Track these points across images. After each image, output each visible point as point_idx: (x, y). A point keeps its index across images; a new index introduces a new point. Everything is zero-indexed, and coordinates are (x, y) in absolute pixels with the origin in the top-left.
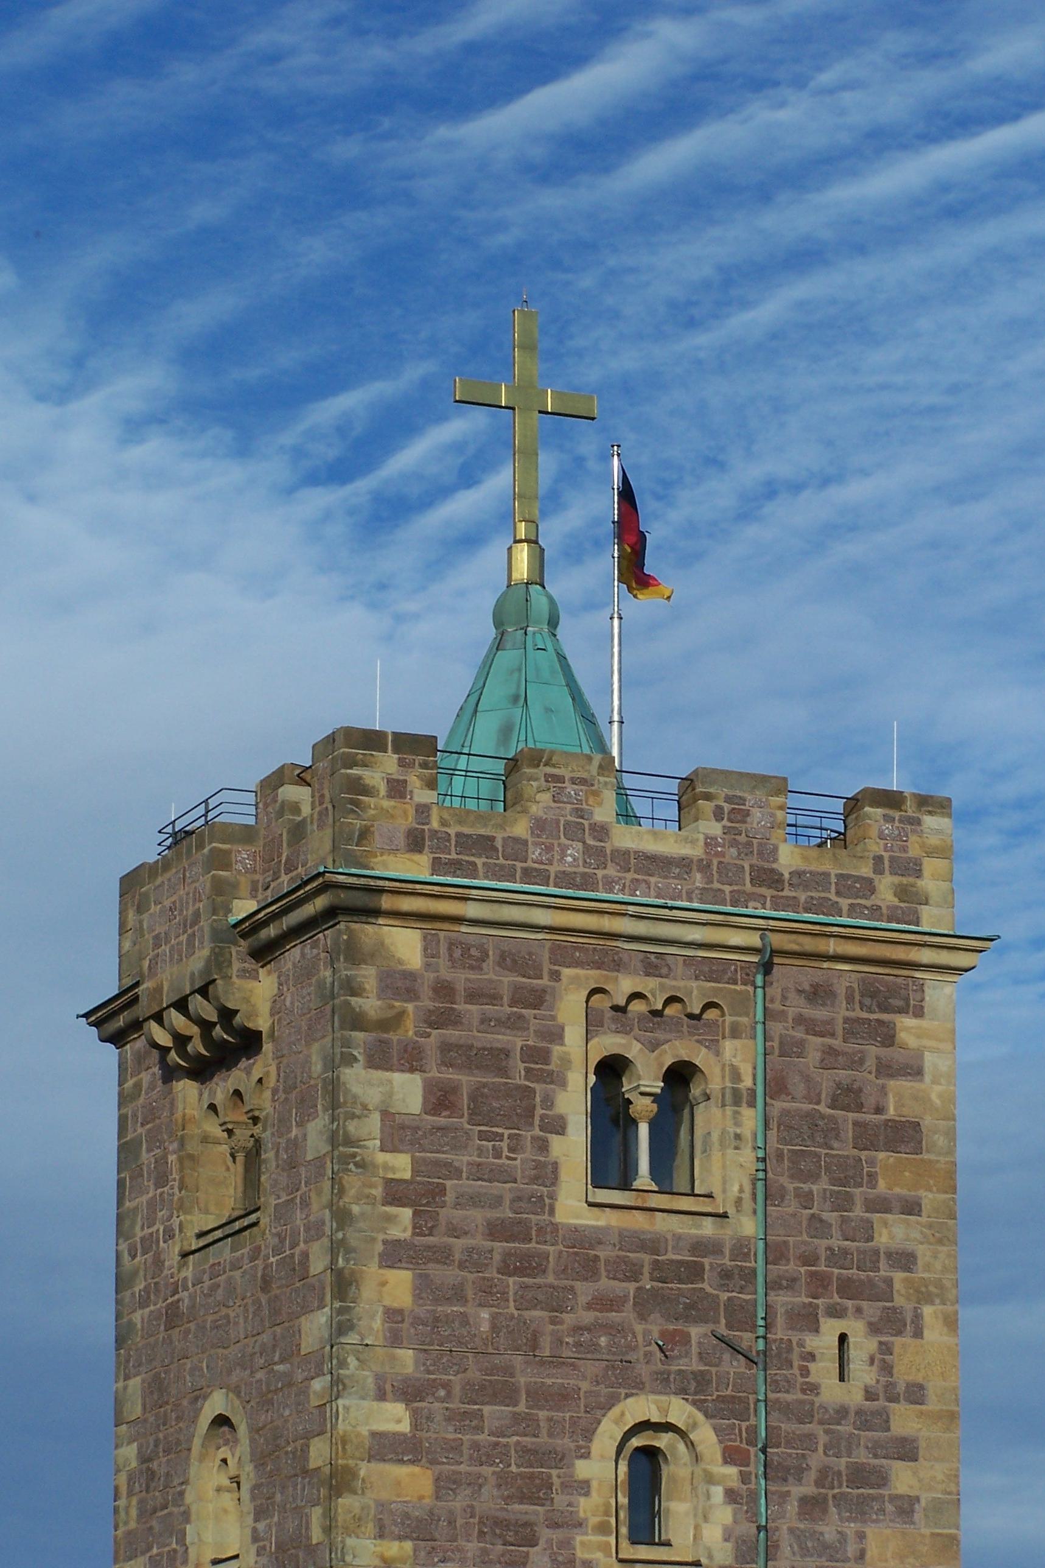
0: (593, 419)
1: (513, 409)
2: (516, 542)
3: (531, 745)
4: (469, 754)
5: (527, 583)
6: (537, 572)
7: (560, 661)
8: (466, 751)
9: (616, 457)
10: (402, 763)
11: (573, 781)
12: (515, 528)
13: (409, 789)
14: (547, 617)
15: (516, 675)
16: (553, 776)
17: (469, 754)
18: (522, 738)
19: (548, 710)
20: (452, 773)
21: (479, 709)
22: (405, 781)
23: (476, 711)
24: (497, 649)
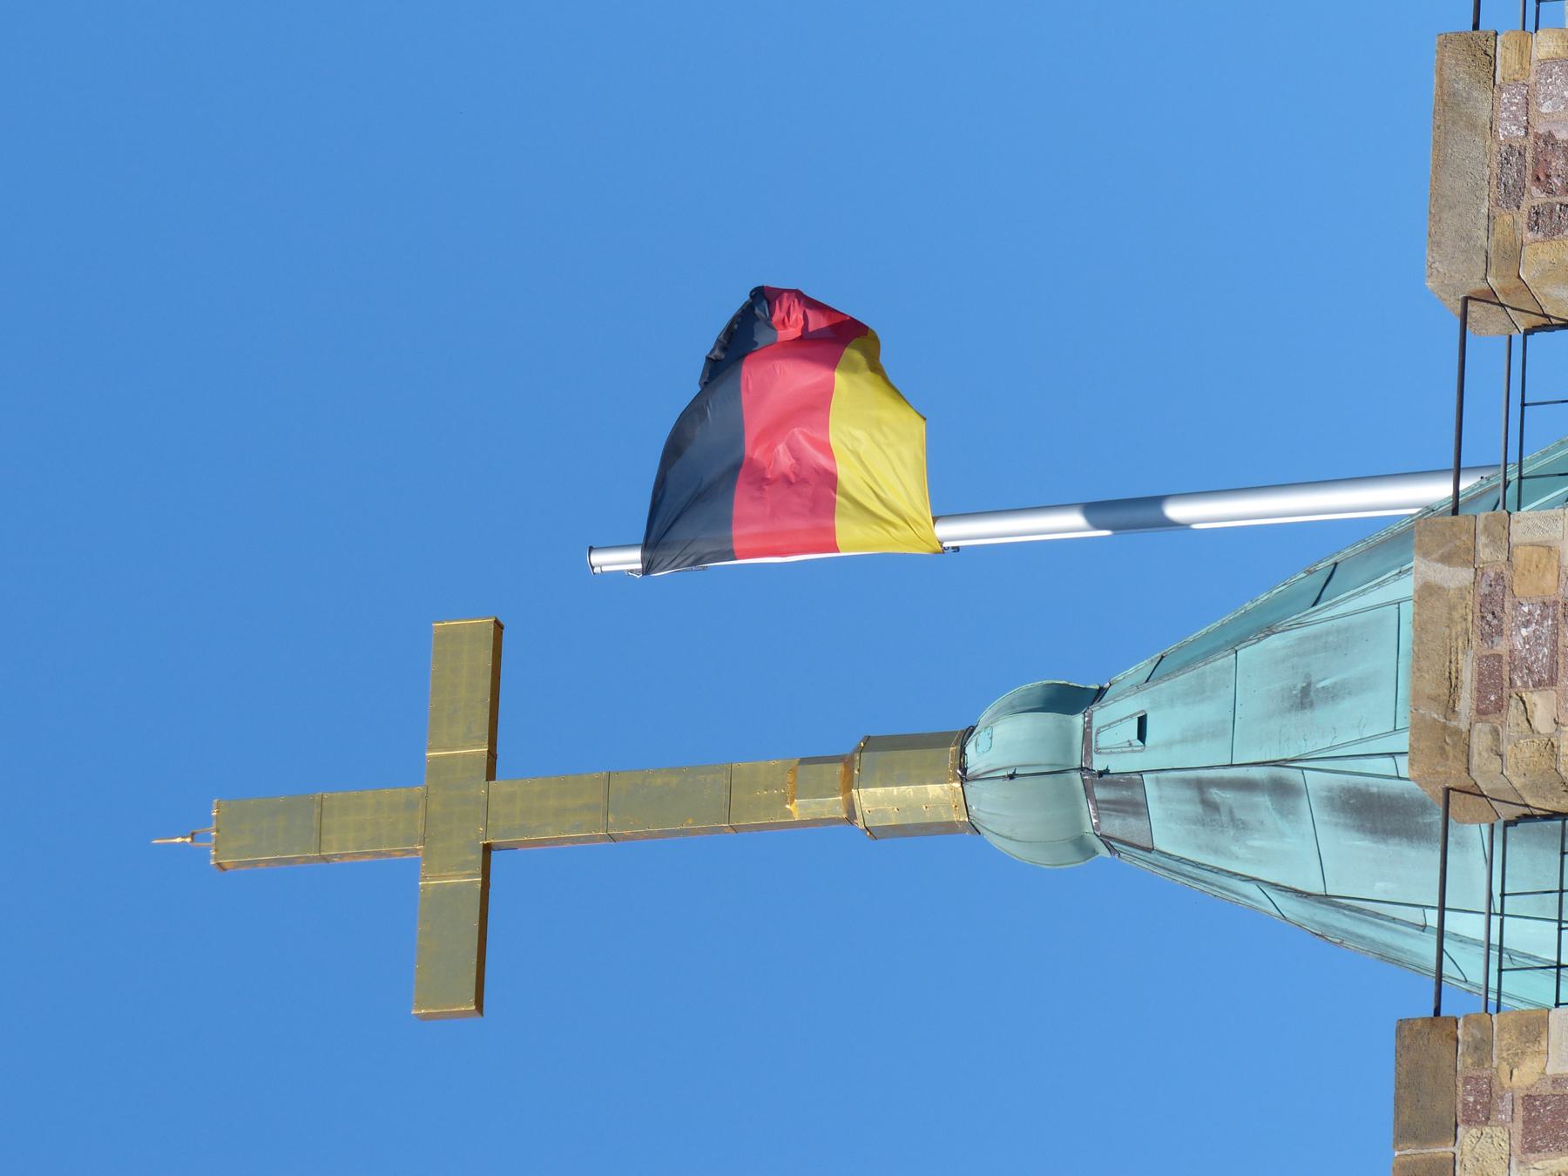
0: (499, 626)
1: (487, 849)
2: (851, 817)
3: (1402, 742)
4: (1442, 909)
5: (964, 779)
6: (931, 754)
7: (1169, 675)
8: (1432, 918)
9: (1439, 491)
10: (1482, 1114)
11: (1492, 632)
12: (1472, 499)
13: (1546, 1089)
14: (1050, 717)
15: (1216, 794)
16: (1481, 691)
17: (1442, 909)
18: (1385, 766)
19: (1305, 699)
20: (1496, 952)
21: (1317, 888)
22: (1529, 1099)
23: (1325, 899)
24: (1150, 850)
